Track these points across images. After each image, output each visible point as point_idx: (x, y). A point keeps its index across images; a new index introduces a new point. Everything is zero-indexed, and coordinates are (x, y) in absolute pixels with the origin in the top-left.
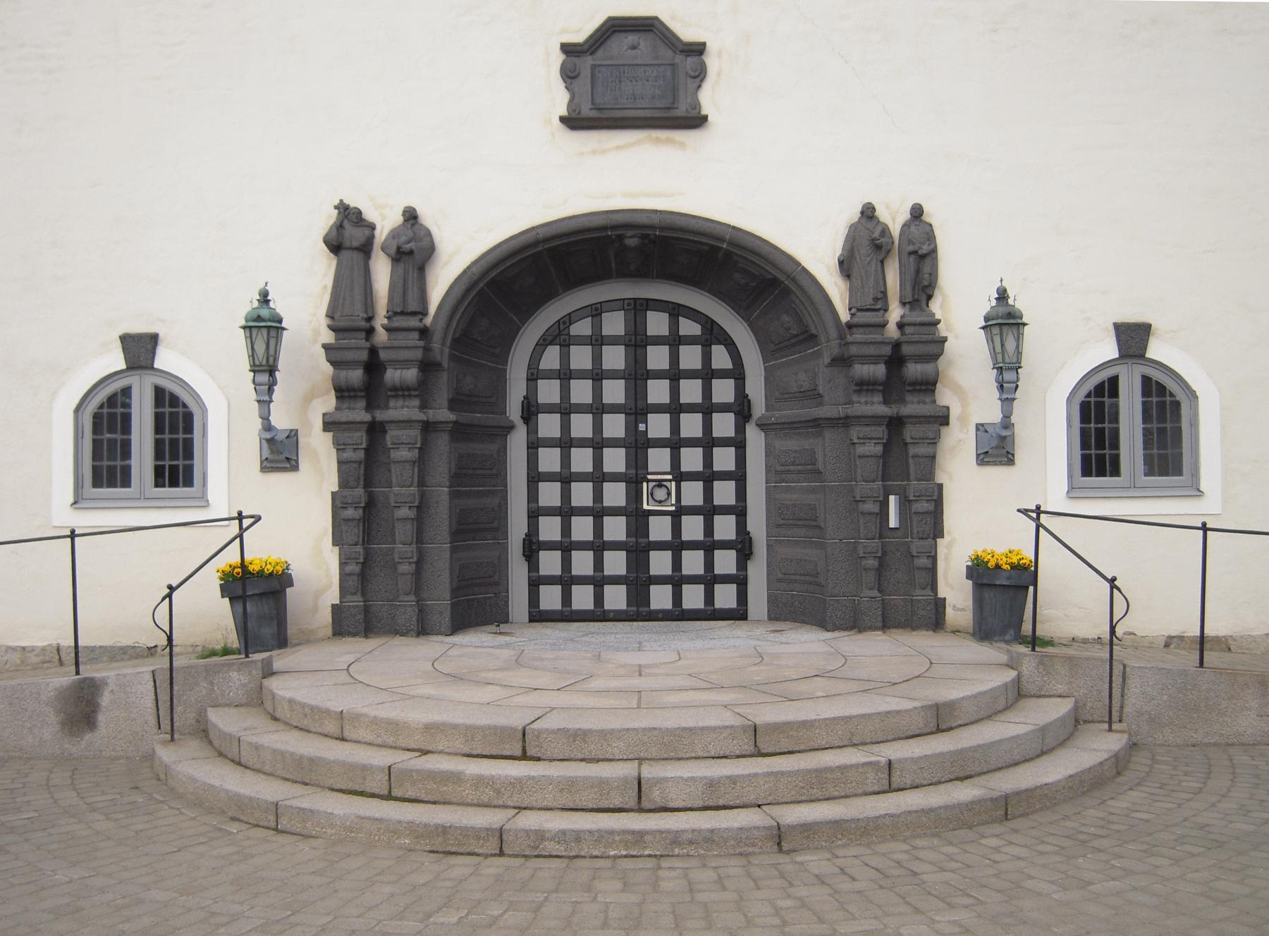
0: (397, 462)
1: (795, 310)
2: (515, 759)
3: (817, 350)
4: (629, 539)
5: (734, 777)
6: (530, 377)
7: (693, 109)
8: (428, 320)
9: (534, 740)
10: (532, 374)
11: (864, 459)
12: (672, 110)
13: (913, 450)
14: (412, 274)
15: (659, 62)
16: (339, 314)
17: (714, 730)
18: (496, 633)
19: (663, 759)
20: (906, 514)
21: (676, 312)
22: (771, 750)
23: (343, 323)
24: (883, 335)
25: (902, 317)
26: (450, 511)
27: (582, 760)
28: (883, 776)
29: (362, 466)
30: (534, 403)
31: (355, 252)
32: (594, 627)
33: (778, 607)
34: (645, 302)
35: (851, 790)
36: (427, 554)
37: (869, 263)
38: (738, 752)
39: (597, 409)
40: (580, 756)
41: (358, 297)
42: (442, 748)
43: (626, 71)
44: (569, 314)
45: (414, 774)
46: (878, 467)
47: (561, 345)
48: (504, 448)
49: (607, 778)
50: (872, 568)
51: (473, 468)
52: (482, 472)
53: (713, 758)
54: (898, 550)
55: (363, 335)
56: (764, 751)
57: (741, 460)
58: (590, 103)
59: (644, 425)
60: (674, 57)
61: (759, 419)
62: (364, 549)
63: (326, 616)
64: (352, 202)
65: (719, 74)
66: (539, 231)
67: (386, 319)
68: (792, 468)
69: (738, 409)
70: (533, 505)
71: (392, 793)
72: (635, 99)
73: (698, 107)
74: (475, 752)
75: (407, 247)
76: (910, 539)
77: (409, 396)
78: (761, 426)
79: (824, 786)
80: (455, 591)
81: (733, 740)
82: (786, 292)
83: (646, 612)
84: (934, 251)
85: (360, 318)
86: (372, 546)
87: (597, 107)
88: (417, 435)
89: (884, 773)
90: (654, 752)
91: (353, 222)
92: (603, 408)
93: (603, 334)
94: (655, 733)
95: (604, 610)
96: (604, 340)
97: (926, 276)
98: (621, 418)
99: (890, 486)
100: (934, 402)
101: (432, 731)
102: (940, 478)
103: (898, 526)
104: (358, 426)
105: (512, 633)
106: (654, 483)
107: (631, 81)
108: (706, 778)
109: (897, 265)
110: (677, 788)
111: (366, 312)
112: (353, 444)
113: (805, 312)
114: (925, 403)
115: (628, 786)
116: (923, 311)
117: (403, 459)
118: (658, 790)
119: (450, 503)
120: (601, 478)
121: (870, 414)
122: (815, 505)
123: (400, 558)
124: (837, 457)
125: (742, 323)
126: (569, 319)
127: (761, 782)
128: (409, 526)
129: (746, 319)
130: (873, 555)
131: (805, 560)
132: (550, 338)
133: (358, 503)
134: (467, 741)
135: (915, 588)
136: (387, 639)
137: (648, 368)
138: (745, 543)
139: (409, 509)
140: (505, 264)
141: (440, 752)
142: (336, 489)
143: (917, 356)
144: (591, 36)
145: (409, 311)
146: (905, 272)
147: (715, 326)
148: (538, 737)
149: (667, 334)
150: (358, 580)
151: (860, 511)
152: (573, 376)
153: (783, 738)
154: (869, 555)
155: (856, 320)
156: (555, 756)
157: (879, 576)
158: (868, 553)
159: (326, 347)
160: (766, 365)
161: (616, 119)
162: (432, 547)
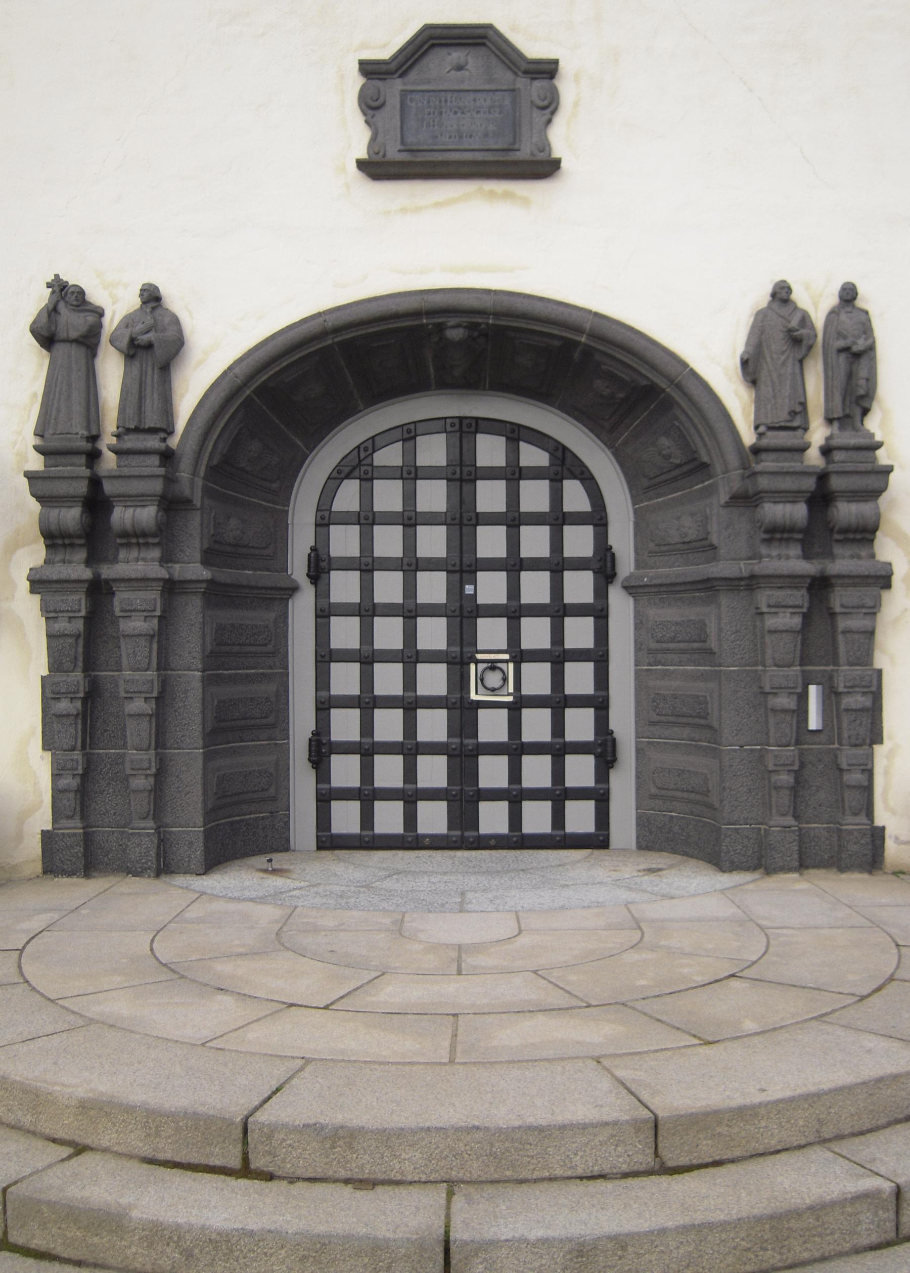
0: (127, 636)
1: (680, 430)
2: (230, 1175)
3: (710, 486)
4: (451, 740)
5: (622, 1238)
6: (320, 521)
7: (541, 151)
8: (174, 442)
9: (262, 1143)
10: (323, 518)
11: (776, 635)
12: (511, 153)
13: (842, 623)
14: (153, 376)
15: (493, 87)
16: (51, 431)
17: (584, 1129)
18: (266, 871)
19: (492, 1182)
20: (832, 711)
21: (515, 435)
22: (684, 1161)
23: (56, 444)
24: (802, 463)
25: (828, 439)
26: (203, 703)
27: (347, 1181)
28: (885, 1215)
29: (81, 642)
30: (325, 557)
31: (74, 345)
32: (402, 859)
33: (651, 833)
34: (473, 422)
35: (831, 1247)
36: (172, 763)
37: (784, 363)
38: (625, 1168)
39: (409, 565)
40: (343, 1174)
41: (78, 408)
42: (108, 1144)
43: (449, 98)
44: (373, 438)
45: (45, 1210)
46: (795, 646)
47: (361, 479)
48: (284, 617)
49: (387, 1241)
50: (786, 785)
51: (239, 644)
52: (253, 649)
53: (581, 1178)
54: (820, 760)
55: (83, 459)
56: (670, 1164)
57: (602, 634)
58: (399, 142)
59: (472, 587)
60: (515, 80)
61: (627, 579)
62: (83, 755)
63: (33, 847)
64: (71, 278)
65: (576, 104)
66: (327, 317)
67: (115, 438)
68: (672, 646)
69: (597, 566)
70: (323, 694)
71: (9, 1236)
72: (461, 137)
73: (547, 148)
74: (161, 1156)
75: (144, 338)
76: (836, 746)
77: (147, 545)
78: (630, 589)
79: (786, 1243)
80: (210, 814)
81: (617, 1146)
82: (668, 404)
83: (473, 837)
84: (871, 348)
85: (79, 436)
86: (97, 751)
87: (408, 147)
88: (155, 600)
89: (888, 1210)
90: (475, 1170)
91: (72, 305)
92: (417, 563)
93: (417, 465)
94: (478, 1135)
95: (418, 835)
96: (419, 472)
97: (862, 382)
98: (440, 578)
99: (810, 672)
100: (873, 556)
101: (92, 1113)
102: (880, 661)
103: (820, 728)
104: (75, 585)
105: (288, 871)
106: (485, 665)
107: (456, 113)
108: (570, 1240)
109: (820, 367)
110: (518, 1259)
111: (88, 427)
112: (68, 611)
113: (692, 431)
114: (859, 557)
115: (426, 1256)
116: (857, 431)
117: (136, 632)
118: (481, 1263)
119: (203, 692)
120: (414, 657)
121: (785, 572)
122: (705, 697)
123: (132, 769)
124: (737, 632)
125: (604, 451)
126: (372, 445)
127: (673, 1244)
128: (145, 724)
129: (610, 445)
130: (787, 768)
131: (688, 771)
132: (347, 470)
133: (74, 693)
134: (148, 1135)
135: (844, 814)
136: (118, 879)
137: (478, 511)
138: (606, 745)
139: (145, 702)
140: (281, 363)
141: (105, 1150)
142: (46, 672)
143: (850, 492)
144: (401, 51)
145: (147, 427)
146: (832, 377)
147: (568, 454)
148: (270, 1137)
149: (504, 464)
150: (75, 798)
151: (769, 706)
152: (377, 521)
153: (705, 1139)
154: (782, 768)
155: (765, 442)
156: (299, 1172)
157: (795, 796)
158: (781, 765)
159: (31, 476)
160: (637, 506)
161: (435, 164)
162: (179, 754)
